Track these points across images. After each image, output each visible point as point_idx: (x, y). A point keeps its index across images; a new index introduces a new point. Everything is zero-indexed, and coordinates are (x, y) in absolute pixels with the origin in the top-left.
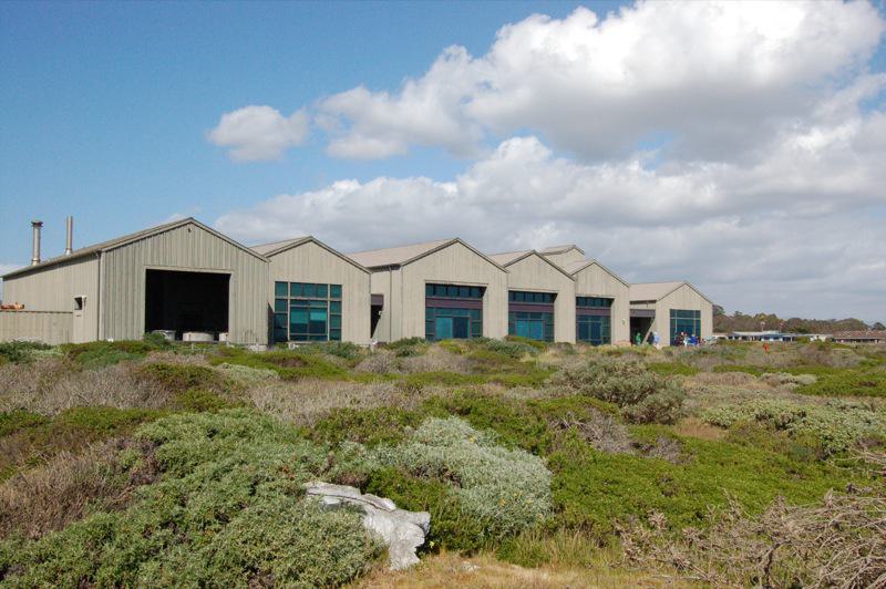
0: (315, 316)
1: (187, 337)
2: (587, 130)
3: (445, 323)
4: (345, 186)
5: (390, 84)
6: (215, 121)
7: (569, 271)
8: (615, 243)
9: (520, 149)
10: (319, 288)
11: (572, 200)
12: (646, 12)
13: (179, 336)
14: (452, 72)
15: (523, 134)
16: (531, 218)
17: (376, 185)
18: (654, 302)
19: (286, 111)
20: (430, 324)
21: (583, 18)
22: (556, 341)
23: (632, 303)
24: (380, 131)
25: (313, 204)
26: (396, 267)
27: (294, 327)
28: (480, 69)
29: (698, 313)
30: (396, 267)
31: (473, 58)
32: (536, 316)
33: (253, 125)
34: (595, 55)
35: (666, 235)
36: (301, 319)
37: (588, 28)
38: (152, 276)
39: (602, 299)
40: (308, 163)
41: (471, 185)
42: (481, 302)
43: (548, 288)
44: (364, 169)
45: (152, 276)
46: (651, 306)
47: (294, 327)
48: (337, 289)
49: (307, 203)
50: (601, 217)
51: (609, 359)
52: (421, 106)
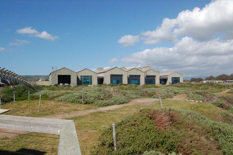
0: (87, 81)
1: (65, 84)
2: (203, 35)
3: (115, 82)
4: (147, 50)
5: (153, 28)
6: (120, 38)
7: (144, 71)
8: (212, 59)
9: (186, 40)
10: (88, 76)
11: (201, 50)
12: (212, 5)
13: (64, 84)
14: (167, 22)
15: (184, 37)
16: (190, 55)
17: (154, 50)
18: (168, 76)
19: (133, 35)
20: (111, 82)
21: (197, 10)
22: (104, 83)
23: (160, 76)
24: (154, 39)
25: (142, 55)
26: (105, 72)
27: (84, 83)
28: (174, 21)
29: (179, 78)
30: (105, 72)
31: (200, 10)
32: (136, 79)
33: (128, 39)
34: (198, 17)
35: (223, 57)
36: (85, 81)
37: (199, 11)
38: (59, 76)
39: (120, 75)
40: (140, 46)
41: (176, 48)
42: (122, 77)
43: (138, 74)
44: (151, 47)
45: (59, 76)
46: (167, 77)
47: (84, 83)
48: (91, 76)
49: (141, 54)
50: (209, 54)
51: (228, 94)
52: (160, 33)
